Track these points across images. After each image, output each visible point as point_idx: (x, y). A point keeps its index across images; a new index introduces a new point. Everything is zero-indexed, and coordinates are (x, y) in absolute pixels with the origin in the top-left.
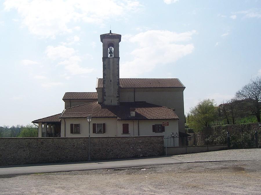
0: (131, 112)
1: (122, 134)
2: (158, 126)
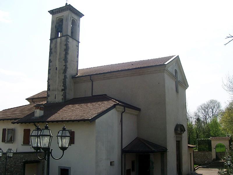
1: (22, 145)
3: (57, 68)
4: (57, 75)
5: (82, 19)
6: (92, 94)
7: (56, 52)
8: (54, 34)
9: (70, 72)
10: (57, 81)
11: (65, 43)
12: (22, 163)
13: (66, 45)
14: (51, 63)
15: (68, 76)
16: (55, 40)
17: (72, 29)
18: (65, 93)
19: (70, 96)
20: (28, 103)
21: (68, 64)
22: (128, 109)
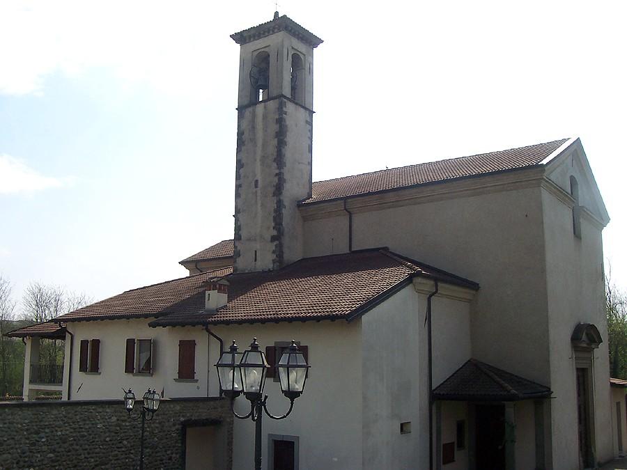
0: (207, 293)
3: (257, 181)
5: (320, 59)
7: (253, 140)
9: (293, 190)
11: (277, 117)
12: (177, 426)
13: (280, 121)
15: (286, 202)
16: (250, 109)
17: (294, 78)
19: (294, 253)
20: (185, 273)
21: (285, 170)
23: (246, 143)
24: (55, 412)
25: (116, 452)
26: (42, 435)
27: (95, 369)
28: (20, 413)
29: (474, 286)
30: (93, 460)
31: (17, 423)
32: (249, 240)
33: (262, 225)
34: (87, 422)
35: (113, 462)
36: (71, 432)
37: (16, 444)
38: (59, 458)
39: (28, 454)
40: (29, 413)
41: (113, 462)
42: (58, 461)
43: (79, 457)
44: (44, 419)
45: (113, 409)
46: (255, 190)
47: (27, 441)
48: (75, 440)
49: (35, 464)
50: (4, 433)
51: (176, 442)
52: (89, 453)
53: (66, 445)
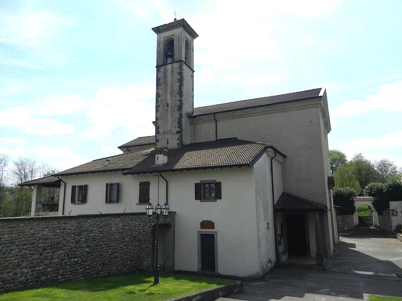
0: (156, 156)
1: (137, 204)
2: (210, 184)
3: (168, 104)
4: (169, 112)
5: (196, 41)
6: (216, 137)
7: (166, 83)
8: (162, 59)
9: (186, 109)
10: (170, 122)
11: (179, 71)
12: (151, 228)
13: (181, 74)
14: (159, 99)
15: (184, 115)
16: (164, 67)
17: (187, 53)
18: (181, 136)
19: (187, 141)
20: (122, 153)
21: (183, 98)
22: (279, 155)
23: (162, 84)
24: (90, 221)
25: (121, 245)
26: (82, 236)
27: (84, 200)
28: (70, 222)
29: (284, 156)
30: (110, 251)
31: (68, 229)
32: (164, 133)
33: (171, 125)
34: (107, 227)
35: (120, 251)
36: (98, 234)
37: (67, 243)
38: (91, 251)
39: (74, 249)
40: (75, 222)
41: (120, 251)
42: (91, 252)
43: (103, 250)
44: (84, 226)
45: (120, 219)
46: (167, 108)
47: (74, 241)
48: (100, 239)
49: (78, 256)
50: (60, 236)
51: (150, 238)
52: (108, 247)
53: (95, 242)
